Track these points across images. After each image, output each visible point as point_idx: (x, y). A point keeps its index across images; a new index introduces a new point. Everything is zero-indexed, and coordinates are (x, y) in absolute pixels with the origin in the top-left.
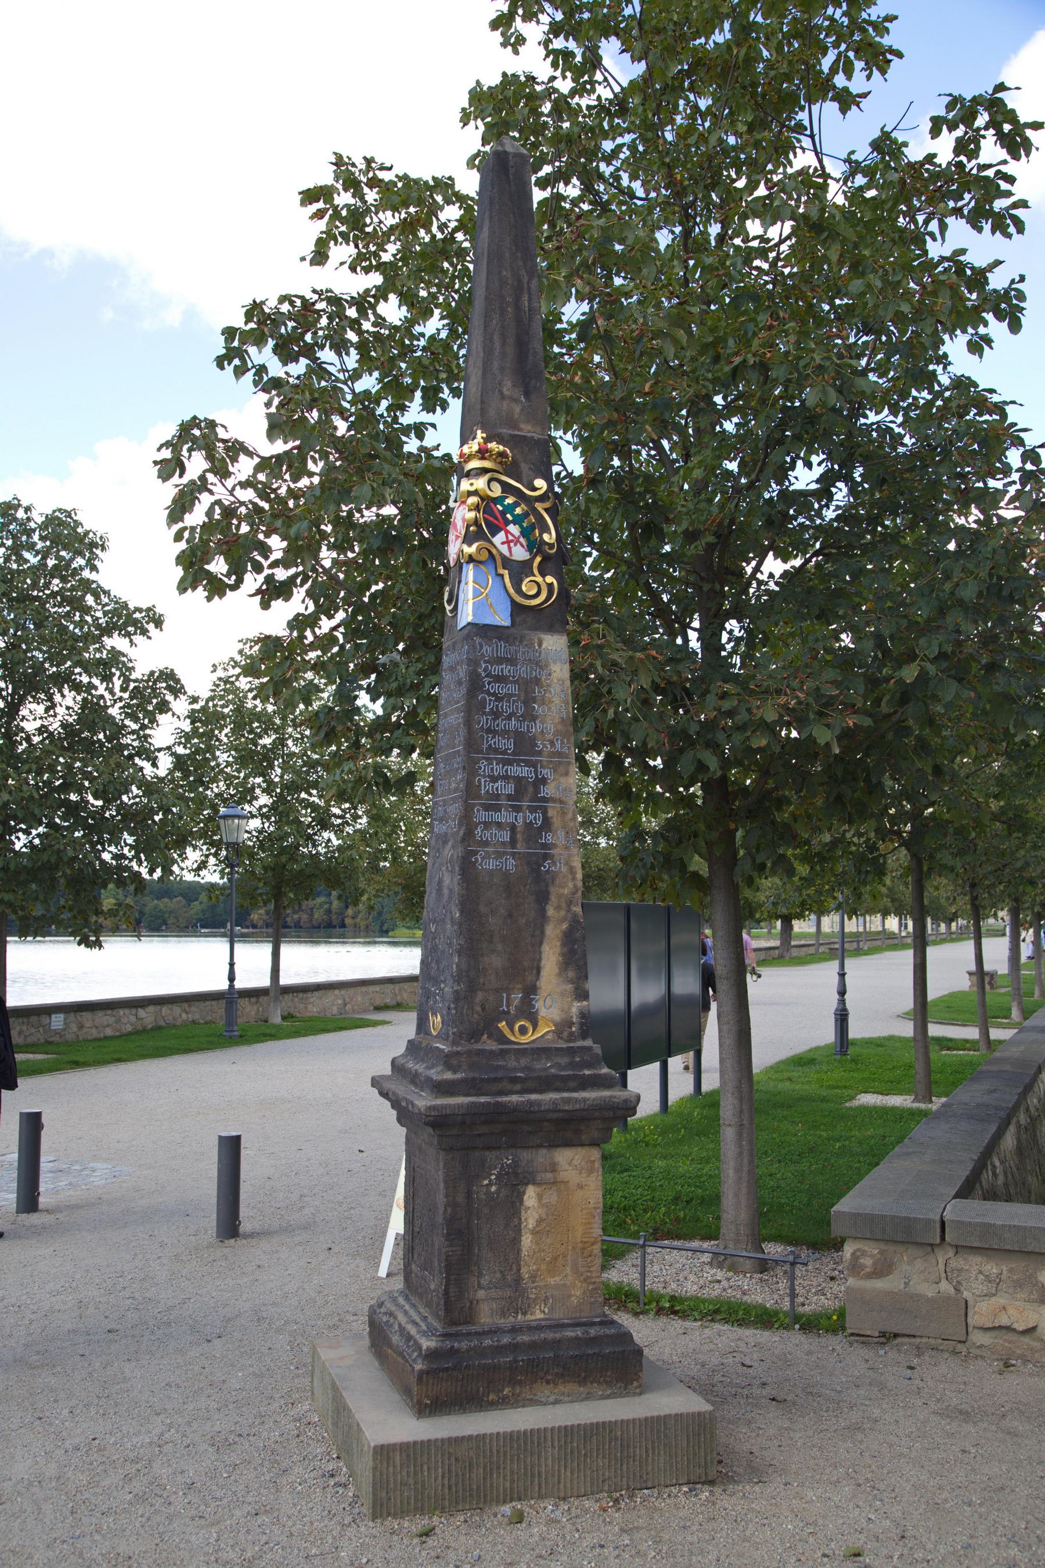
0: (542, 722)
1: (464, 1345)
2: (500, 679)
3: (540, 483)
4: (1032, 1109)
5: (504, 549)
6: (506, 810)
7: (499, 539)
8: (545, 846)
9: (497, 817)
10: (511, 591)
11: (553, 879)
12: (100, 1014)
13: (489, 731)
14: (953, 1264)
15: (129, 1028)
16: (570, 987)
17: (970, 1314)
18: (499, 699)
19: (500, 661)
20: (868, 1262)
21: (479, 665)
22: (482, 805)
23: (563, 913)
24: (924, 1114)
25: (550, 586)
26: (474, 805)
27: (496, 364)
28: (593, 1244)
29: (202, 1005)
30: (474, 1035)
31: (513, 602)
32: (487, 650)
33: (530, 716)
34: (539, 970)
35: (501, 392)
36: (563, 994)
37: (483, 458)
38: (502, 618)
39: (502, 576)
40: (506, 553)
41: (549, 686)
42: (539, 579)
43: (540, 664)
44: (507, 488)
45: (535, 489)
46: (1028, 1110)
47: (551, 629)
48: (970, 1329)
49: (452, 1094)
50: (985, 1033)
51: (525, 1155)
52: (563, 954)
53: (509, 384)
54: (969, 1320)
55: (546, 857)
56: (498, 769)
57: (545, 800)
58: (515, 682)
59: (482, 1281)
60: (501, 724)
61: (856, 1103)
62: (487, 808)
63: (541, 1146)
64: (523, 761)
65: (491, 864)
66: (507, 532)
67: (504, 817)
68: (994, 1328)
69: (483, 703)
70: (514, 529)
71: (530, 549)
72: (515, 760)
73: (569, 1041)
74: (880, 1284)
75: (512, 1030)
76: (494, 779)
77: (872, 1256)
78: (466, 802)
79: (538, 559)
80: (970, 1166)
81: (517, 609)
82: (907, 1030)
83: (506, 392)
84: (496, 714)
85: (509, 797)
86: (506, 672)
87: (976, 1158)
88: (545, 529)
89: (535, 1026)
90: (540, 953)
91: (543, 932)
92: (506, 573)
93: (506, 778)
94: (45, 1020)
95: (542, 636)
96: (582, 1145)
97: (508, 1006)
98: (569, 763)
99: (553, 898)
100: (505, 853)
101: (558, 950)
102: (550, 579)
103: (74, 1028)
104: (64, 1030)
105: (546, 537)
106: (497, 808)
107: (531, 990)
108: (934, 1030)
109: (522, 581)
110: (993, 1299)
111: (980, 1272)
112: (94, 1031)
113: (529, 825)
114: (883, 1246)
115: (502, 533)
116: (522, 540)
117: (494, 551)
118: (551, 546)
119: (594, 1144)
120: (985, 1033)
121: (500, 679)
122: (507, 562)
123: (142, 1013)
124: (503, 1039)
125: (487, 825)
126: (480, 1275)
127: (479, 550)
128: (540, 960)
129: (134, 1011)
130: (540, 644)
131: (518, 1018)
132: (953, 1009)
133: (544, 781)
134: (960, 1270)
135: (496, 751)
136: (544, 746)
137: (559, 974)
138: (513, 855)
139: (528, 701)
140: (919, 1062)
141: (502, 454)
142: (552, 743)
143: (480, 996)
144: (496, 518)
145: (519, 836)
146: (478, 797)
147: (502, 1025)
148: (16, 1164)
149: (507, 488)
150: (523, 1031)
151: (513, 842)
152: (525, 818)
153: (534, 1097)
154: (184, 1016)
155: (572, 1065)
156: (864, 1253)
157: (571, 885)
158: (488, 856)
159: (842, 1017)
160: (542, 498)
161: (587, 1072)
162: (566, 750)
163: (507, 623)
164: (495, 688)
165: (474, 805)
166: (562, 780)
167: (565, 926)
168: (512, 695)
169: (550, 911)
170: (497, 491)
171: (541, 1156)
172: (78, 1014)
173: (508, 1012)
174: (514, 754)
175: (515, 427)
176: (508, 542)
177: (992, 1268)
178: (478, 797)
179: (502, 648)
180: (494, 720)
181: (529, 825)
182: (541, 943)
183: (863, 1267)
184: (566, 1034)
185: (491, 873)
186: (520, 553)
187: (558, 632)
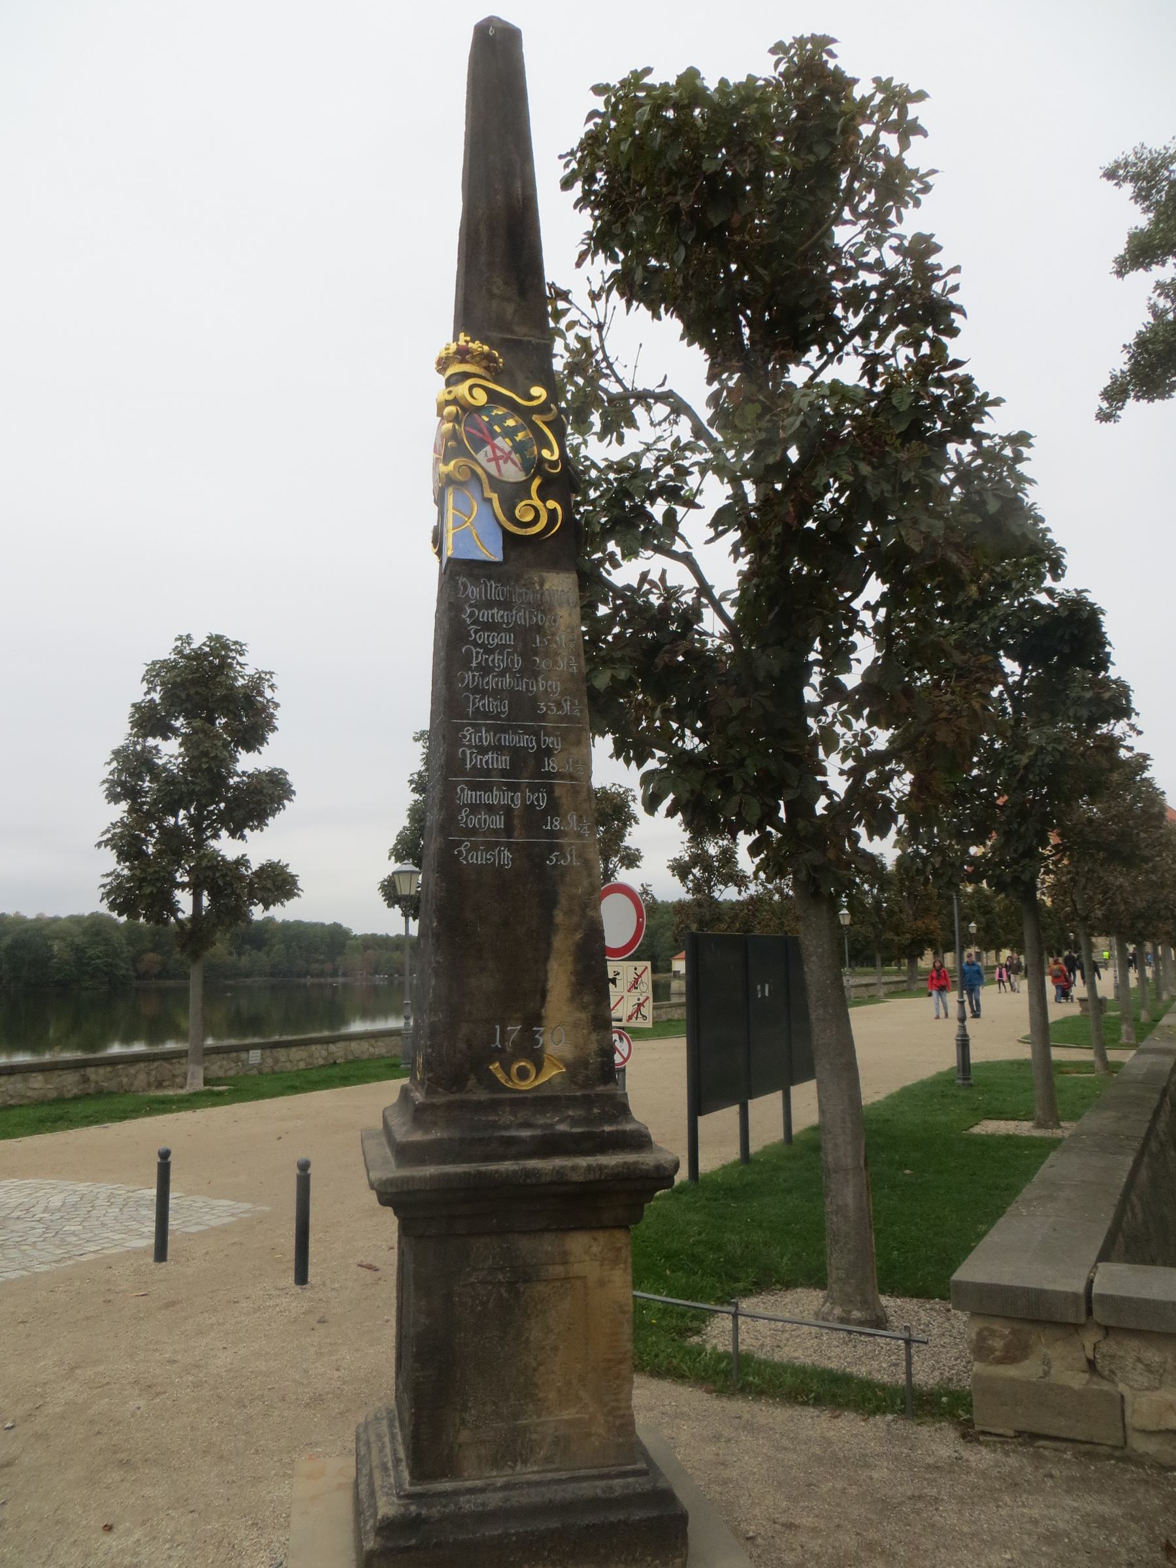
0: (546, 679)
1: (435, 1512)
2: (490, 627)
3: (538, 391)
4: (1161, 1134)
5: (492, 468)
6: (499, 789)
7: (483, 456)
8: (552, 834)
9: (486, 798)
10: (502, 518)
11: (563, 876)
12: (294, 1049)
13: (476, 690)
14: (1104, 1348)
15: (321, 1062)
16: (583, 1016)
17: (1128, 1413)
18: (489, 651)
19: (489, 604)
20: (998, 1344)
21: (463, 610)
22: (466, 782)
23: (575, 919)
24: (1054, 1144)
25: (552, 513)
26: (458, 783)
27: (483, 259)
28: (621, 1362)
29: (387, 1039)
30: (456, 1081)
31: (506, 534)
32: (473, 592)
33: (529, 670)
34: (544, 993)
35: (489, 291)
36: (576, 1025)
37: (463, 361)
38: (492, 552)
39: (490, 500)
40: (494, 472)
41: (553, 634)
42: (537, 502)
43: (542, 607)
44: (493, 397)
45: (532, 398)
46: (1158, 1136)
47: (555, 565)
48: (1129, 1432)
49: (422, 1162)
50: (1102, 1056)
51: (525, 1244)
52: (575, 973)
53: (500, 282)
54: (1128, 1420)
55: (552, 847)
56: (487, 738)
57: (549, 775)
58: (509, 631)
59: (467, 1417)
60: (491, 681)
61: (976, 1130)
62: (474, 786)
63: (546, 1230)
64: (520, 727)
65: (478, 858)
66: (494, 447)
67: (496, 797)
68: (1160, 1432)
69: (468, 657)
70: (504, 444)
71: (526, 467)
72: (511, 727)
73: (583, 1087)
74: (1011, 1371)
75: (508, 1073)
76: (482, 750)
77: (1002, 1337)
78: (445, 779)
79: (536, 483)
80: (1112, 1212)
81: (510, 541)
82: (1026, 1053)
83: (496, 291)
84: (485, 670)
85: (503, 773)
86: (498, 619)
87: (1116, 1202)
88: (544, 443)
89: (539, 1069)
90: (546, 972)
91: (549, 945)
92: (495, 497)
93: (498, 749)
94: (243, 1055)
95: (545, 574)
96: (603, 1227)
97: (502, 1041)
98: (582, 730)
99: (563, 901)
100: (498, 844)
101: (570, 967)
102: (551, 504)
103: (270, 1061)
104: (260, 1064)
105: (546, 453)
106: (487, 787)
107: (534, 1020)
108: (1057, 1054)
109: (515, 507)
110: (1157, 1393)
111: (1139, 1360)
112: (288, 1065)
113: (529, 808)
114: (1017, 1326)
115: (488, 448)
116: (513, 456)
117: (479, 471)
118: (553, 464)
119: (623, 1226)
120: (1102, 1056)
121: (490, 627)
122: (496, 483)
123: (332, 1048)
124: (493, 1084)
125: (474, 808)
126: (465, 1408)
127: (458, 468)
128: (546, 980)
129: (325, 1047)
130: (542, 585)
131: (515, 1057)
132: (1072, 1033)
133: (549, 752)
134: (1113, 1357)
135: (486, 715)
136: (549, 708)
137: (572, 999)
138: (509, 846)
139: (528, 653)
140: (1040, 1085)
141: (488, 357)
142: (559, 706)
143: (465, 1029)
144: (481, 431)
145: (516, 822)
146: (462, 772)
147: (495, 1067)
148: (155, 1199)
149: (493, 397)
150: (523, 1074)
151: (508, 830)
152: (524, 799)
153: (533, 1164)
154: (371, 1049)
155: (587, 1121)
156: (992, 1333)
157: (586, 883)
158: (474, 847)
159: (964, 1043)
160: (543, 409)
161: (607, 1128)
162: (577, 713)
163: (498, 557)
164: (483, 637)
165: (458, 783)
166: (574, 750)
167: (578, 936)
168: (506, 646)
169: (559, 917)
170: (481, 398)
171: (548, 1244)
172: (274, 1051)
173: (503, 1050)
174: (508, 718)
175: (512, 332)
176: (496, 459)
177: (1153, 1356)
178: (462, 772)
179: (494, 589)
180: (483, 677)
181: (529, 808)
182: (547, 959)
183: (992, 1350)
184: (580, 1078)
185: (479, 868)
186: (512, 473)
187: (567, 570)
